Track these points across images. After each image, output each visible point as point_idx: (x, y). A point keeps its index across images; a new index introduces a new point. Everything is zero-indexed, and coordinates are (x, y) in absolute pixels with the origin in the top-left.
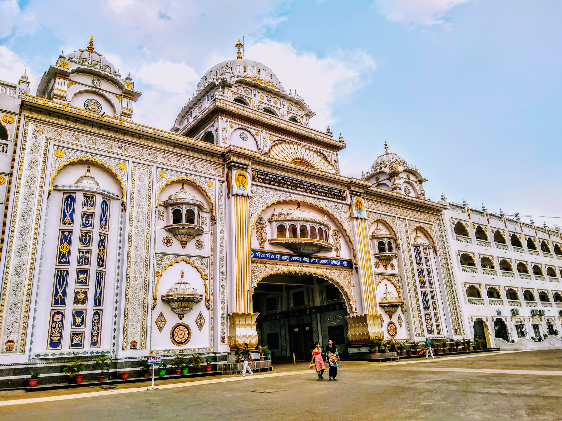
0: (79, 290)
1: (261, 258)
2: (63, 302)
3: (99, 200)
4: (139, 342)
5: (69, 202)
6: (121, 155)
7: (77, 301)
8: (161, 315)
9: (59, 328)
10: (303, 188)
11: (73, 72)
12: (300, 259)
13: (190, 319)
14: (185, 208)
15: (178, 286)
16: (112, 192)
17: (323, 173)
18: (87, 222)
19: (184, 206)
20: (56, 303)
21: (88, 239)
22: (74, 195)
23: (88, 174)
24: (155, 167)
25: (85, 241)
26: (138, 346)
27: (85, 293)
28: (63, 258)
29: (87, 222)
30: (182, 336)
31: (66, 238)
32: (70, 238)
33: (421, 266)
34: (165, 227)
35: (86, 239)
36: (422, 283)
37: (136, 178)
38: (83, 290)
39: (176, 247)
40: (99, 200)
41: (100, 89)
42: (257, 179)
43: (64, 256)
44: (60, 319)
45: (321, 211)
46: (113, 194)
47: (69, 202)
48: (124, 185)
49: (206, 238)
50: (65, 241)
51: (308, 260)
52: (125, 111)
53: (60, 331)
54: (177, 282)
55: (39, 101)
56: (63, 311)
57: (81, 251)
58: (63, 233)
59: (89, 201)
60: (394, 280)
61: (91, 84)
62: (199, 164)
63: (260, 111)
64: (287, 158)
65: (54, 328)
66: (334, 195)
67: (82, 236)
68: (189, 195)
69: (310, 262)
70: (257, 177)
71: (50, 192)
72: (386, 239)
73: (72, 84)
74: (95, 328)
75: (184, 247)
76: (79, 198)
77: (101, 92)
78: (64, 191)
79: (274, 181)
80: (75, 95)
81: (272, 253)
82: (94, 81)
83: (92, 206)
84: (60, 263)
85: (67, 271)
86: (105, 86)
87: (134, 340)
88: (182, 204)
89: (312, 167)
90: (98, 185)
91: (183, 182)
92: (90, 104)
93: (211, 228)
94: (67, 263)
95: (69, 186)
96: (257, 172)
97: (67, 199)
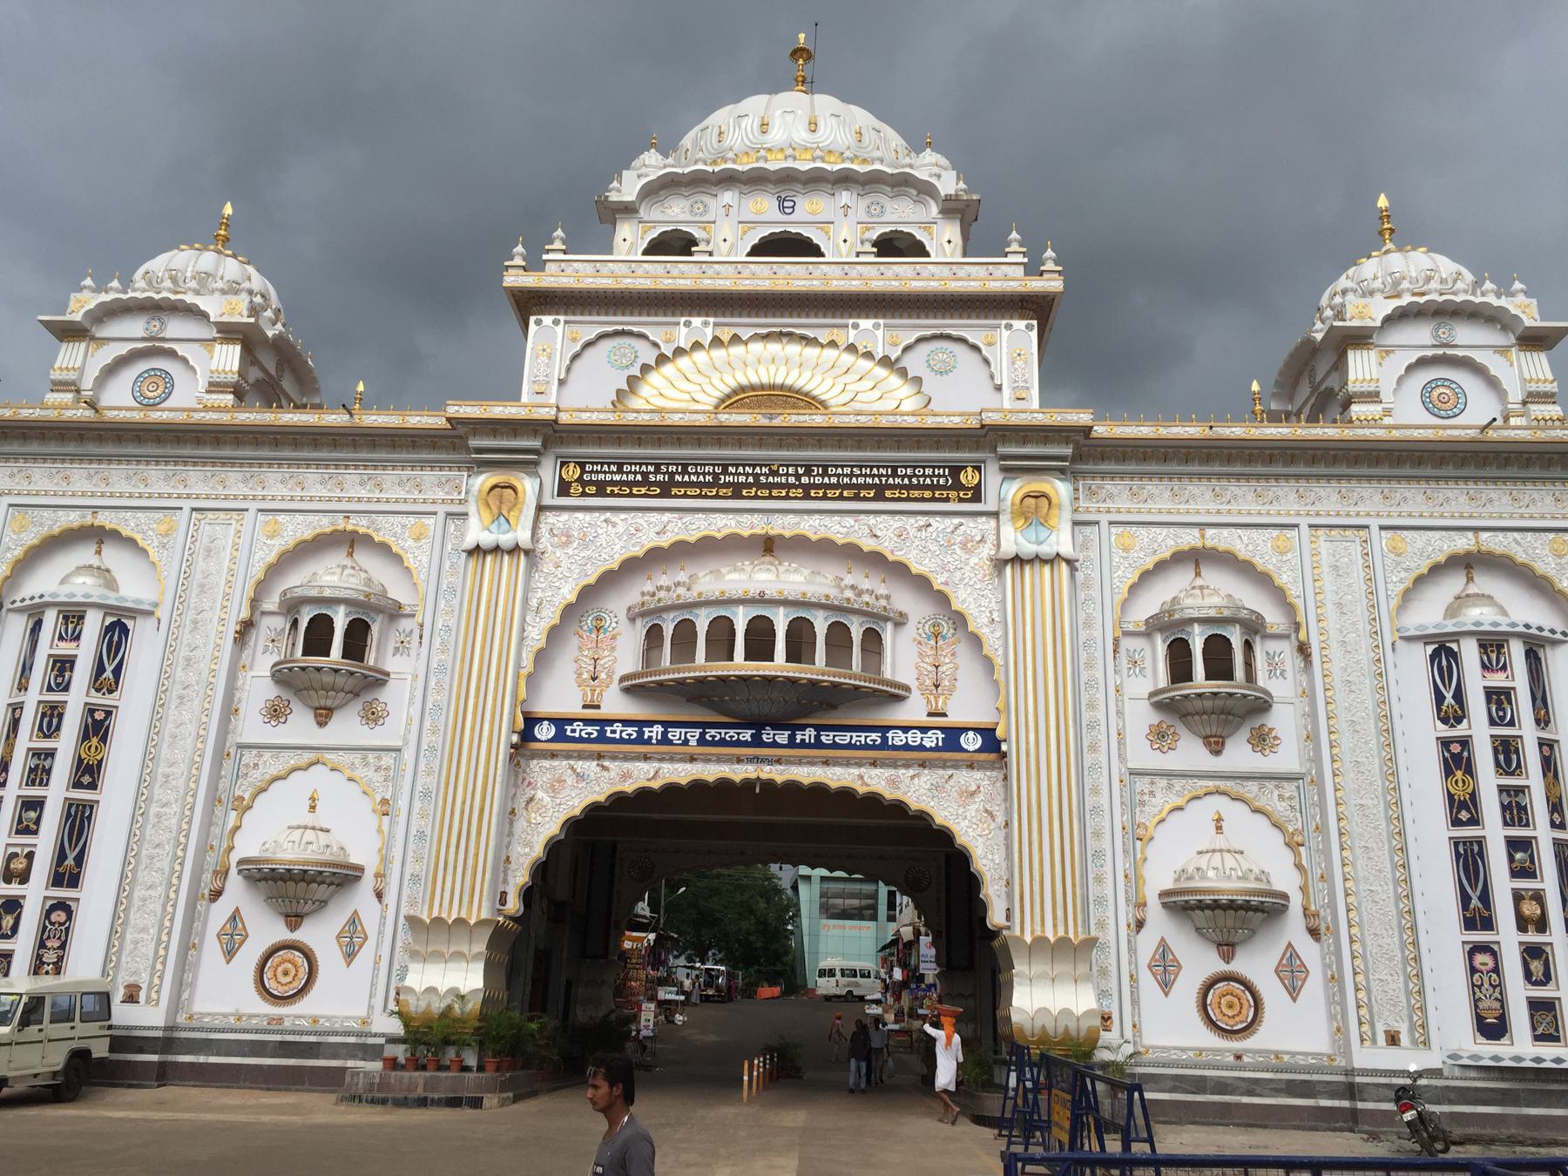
0: (18, 850)
1: (581, 740)
2: (1488, 924)
3: (1517, 651)
4: (144, 986)
5: (1444, 663)
6: (369, 500)
7: (1522, 924)
8: (1164, 947)
9: (1494, 987)
10: (770, 486)
11: (1389, 320)
12: (747, 735)
13: (320, 934)
14: (1201, 634)
15: (1203, 862)
16: (1547, 625)
17: (863, 419)
18: (60, 680)
19: (342, 610)
20: (1470, 924)
21: (55, 721)
22: (1454, 646)
23: (1472, 589)
24: (1375, 529)
25: (1509, 766)
26: (1405, 1039)
27: (30, 856)
28: (1463, 809)
29: (60, 680)
30: (289, 979)
31: (1457, 758)
32: (1469, 759)
33: (1461, 730)
34: (1152, 695)
35: (50, 723)
36: (1463, 805)
37: (1325, 569)
38: (27, 850)
39: (1190, 753)
40: (93, 625)
41: (164, 340)
42: (576, 488)
43: (1463, 805)
44: (1491, 964)
45: (851, 554)
46: (1553, 631)
47: (1444, 663)
48: (1293, 591)
49: (1283, 720)
50: (1459, 768)
51: (782, 737)
52: (1533, 387)
53: (1497, 995)
54: (295, 824)
55: (802, 418)
56: (1495, 947)
57: (1502, 789)
58: (91, 712)
59: (1494, 656)
60: (1270, 798)
61: (141, 334)
62: (390, 476)
63: (862, 259)
64: (698, 396)
65: (1479, 987)
66: (932, 488)
67: (44, 715)
68: (1216, 593)
69: (792, 744)
70: (580, 480)
71: (1116, 641)
72: (1197, 628)
73: (1388, 353)
74: (49, 944)
75: (321, 724)
76: (1470, 653)
77: (1460, 353)
78: (1426, 639)
79: (645, 482)
80: (1400, 380)
81: (626, 723)
82: (1437, 330)
83: (1504, 668)
84: (77, 785)
85: (1480, 844)
86: (1466, 336)
87: (132, 980)
88: (1192, 621)
89: (810, 401)
90: (1504, 613)
91: (1196, 558)
92: (1435, 393)
93: (1304, 679)
94: (1475, 821)
95: (1475, 624)
96: (582, 465)
97: (1435, 656)
